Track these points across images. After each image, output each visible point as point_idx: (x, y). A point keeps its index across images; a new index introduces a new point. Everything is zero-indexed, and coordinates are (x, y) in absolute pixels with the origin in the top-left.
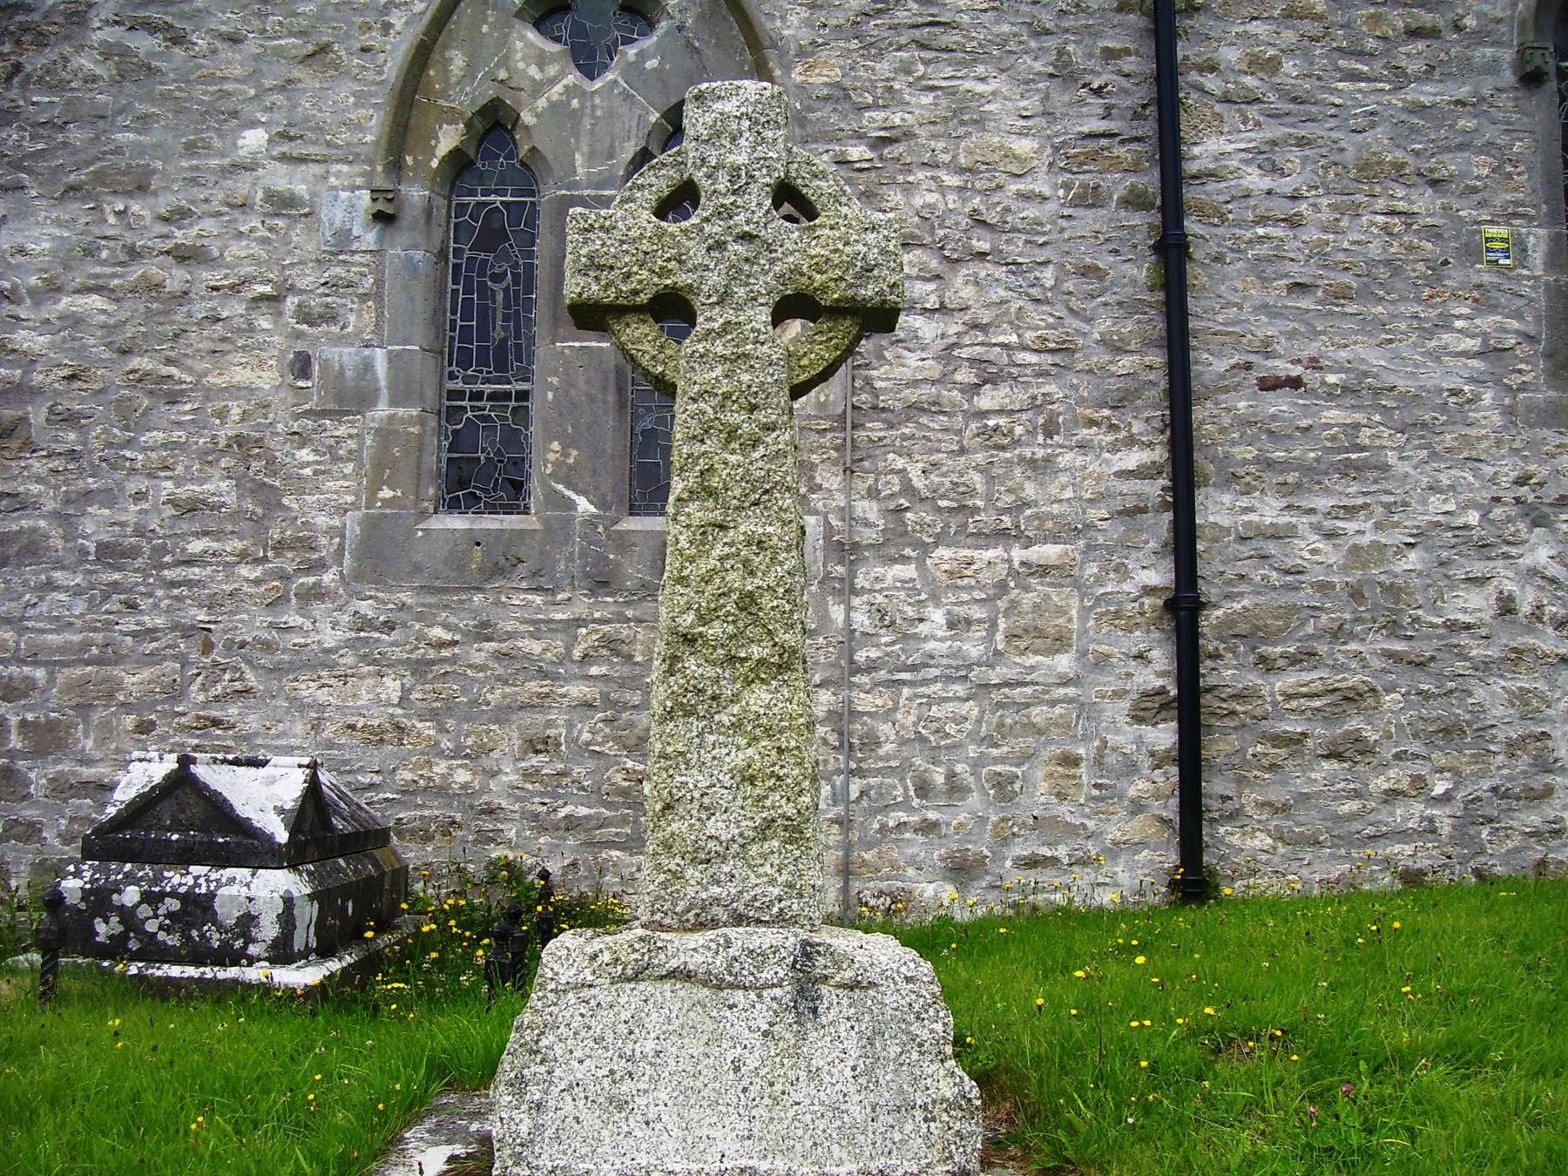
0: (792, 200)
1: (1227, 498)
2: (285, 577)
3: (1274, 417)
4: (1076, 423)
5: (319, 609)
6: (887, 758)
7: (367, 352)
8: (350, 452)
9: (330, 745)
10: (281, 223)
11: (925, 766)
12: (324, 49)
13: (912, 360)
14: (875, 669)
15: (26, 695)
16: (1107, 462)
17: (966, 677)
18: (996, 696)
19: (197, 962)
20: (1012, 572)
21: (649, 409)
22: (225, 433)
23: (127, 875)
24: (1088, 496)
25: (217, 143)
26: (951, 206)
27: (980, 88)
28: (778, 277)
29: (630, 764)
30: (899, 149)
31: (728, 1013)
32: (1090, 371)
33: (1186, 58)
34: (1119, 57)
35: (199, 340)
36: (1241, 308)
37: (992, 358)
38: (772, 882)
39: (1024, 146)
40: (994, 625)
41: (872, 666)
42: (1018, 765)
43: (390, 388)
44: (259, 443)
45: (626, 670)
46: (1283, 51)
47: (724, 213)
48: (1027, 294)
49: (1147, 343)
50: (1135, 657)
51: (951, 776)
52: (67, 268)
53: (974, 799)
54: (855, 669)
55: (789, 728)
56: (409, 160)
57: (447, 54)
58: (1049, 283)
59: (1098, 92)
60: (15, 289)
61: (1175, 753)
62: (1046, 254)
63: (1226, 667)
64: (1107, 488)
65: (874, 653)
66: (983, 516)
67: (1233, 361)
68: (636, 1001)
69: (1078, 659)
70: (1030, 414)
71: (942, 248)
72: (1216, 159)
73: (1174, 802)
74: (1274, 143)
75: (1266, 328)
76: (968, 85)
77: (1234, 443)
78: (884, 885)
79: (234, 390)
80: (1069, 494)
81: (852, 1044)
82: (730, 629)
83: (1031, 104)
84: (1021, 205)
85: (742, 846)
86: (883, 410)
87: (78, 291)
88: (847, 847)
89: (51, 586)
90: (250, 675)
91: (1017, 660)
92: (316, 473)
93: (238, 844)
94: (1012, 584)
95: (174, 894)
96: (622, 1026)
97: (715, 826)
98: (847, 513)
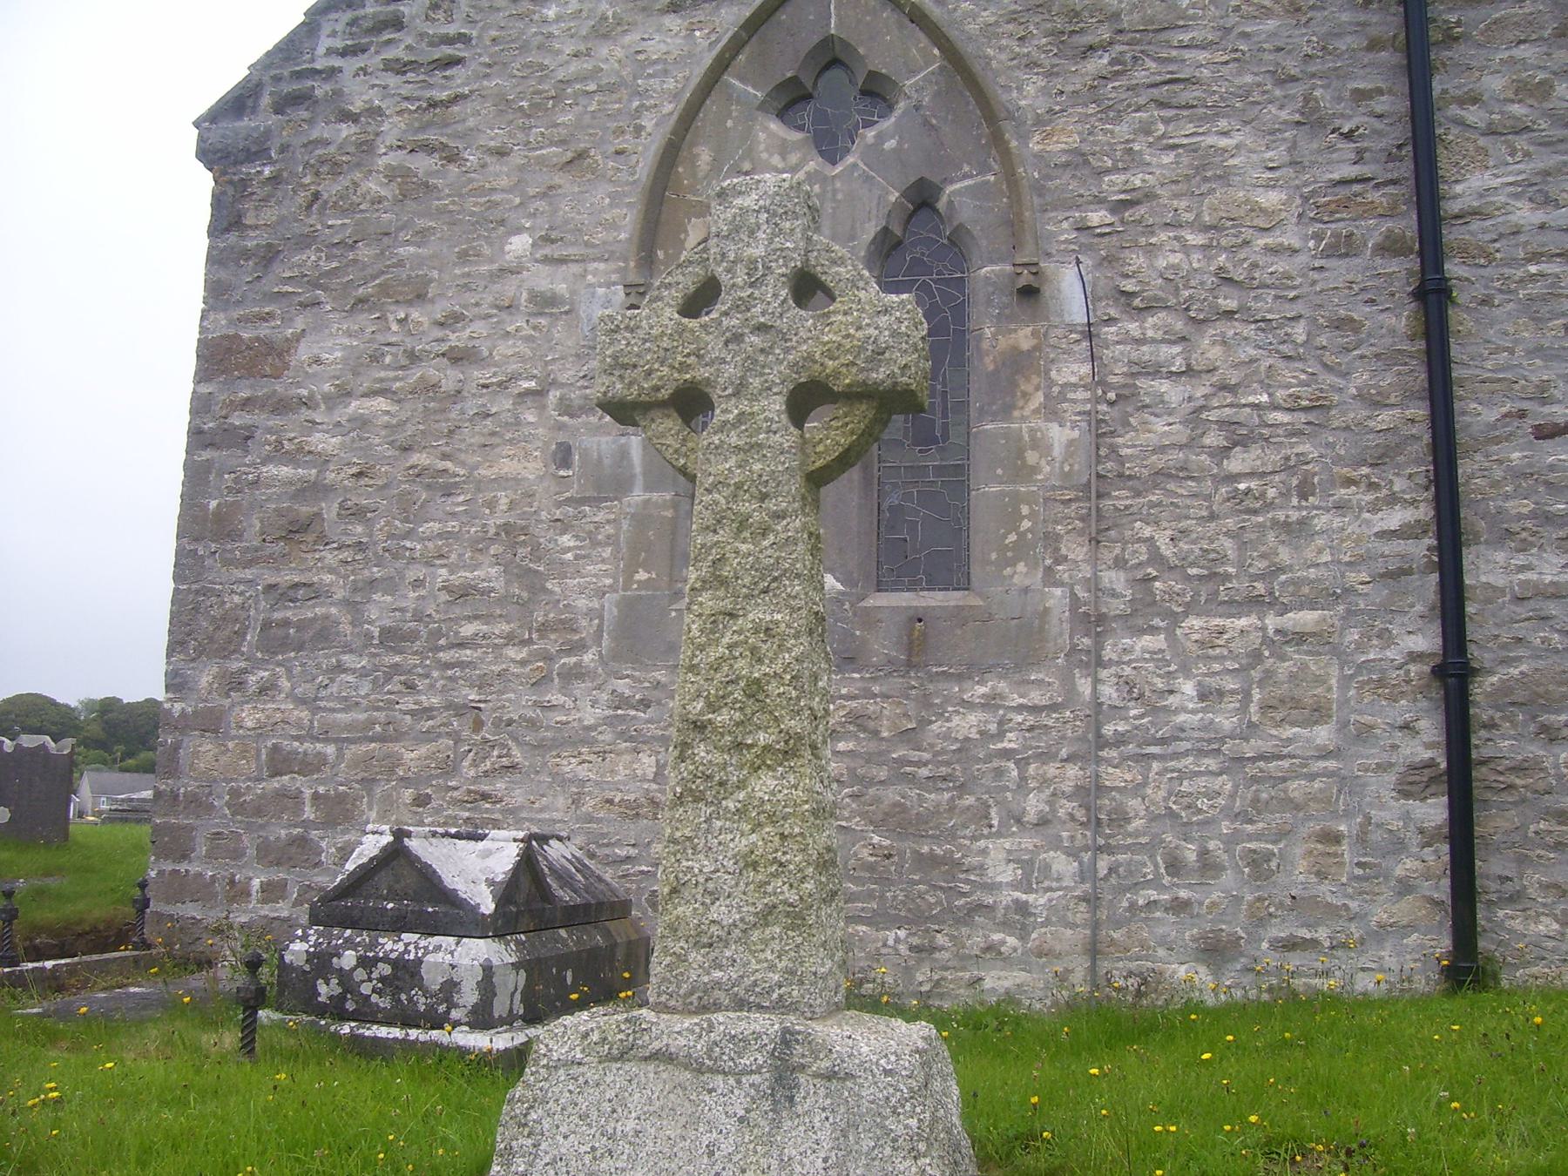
0: (807, 287)
1: (1500, 556)
2: (548, 658)
3: (1552, 468)
4: (1333, 484)
5: (579, 688)
6: (1137, 834)
7: (623, 440)
8: (608, 537)
9: (590, 819)
10: (543, 321)
11: (1176, 842)
12: (581, 155)
13: (1159, 426)
14: (1124, 743)
15: (319, 770)
16: (1368, 522)
17: (1218, 750)
18: (1250, 770)
19: (407, 1024)
20: (1266, 641)
21: (895, 485)
22: (494, 522)
23: (347, 940)
24: (1347, 559)
25: (487, 250)
26: (1195, 265)
27: (1224, 142)
28: (790, 367)
29: (876, 839)
30: (1142, 210)
31: (707, 1098)
32: (1347, 428)
33: (1445, 91)
34: (1371, 98)
35: (471, 436)
36: (1512, 352)
37: (1242, 419)
38: (772, 968)
39: (1271, 199)
40: (1247, 695)
41: (1120, 740)
42: (1275, 842)
43: (644, 474)
44: (524, 530)
45: (873, 746)
46: (1555, 73)
47: (743, 306)
48: (1277, 352)
49: (1408, 396)
50: (1401, 728)
51: (1204, 853)
52: (356, 374)
53: (1227, 878)
54: (1102, 742)
55: (793, 814)
56: (660, 254)
57: (696, 150)
58: (1301, 339)
59: (1349, 136)
60: (311, 396)
61: (1446, 830)
62: (1298, 308)
63: (1503, 737)
64: (1368, 550)
65: (1122, 727)
66: (1235, 584)
67: (1504, 410)
68: (621, 1082)
69: (1339, 730)
70: (1283, 476)
71: (1187, 309)
72: (1481, 196)
73: (1446, 882)
74: (1546, 173)
75: (1540, 372)
76: (1210, 140)
77: (1507, 497)
78: (1133, 965)
79: (501, 481)
80: (1326, 557)
81: (825, 1135)
82: (737, 716)
83: (1277, 155)
84: (1270, 259)
85: (744, 931)
86: (1130, 477)
87: (364, 395)
88: (1096, 926)
89: (340, 668)
90: (516, 752)
91: (1273, 732)
92: (577, 557)
93: (446, 914)
94: (1267, 653)
95: (386, 959)
96: (606, 1104)
97: (719, 911)
98: (1094, 585)
